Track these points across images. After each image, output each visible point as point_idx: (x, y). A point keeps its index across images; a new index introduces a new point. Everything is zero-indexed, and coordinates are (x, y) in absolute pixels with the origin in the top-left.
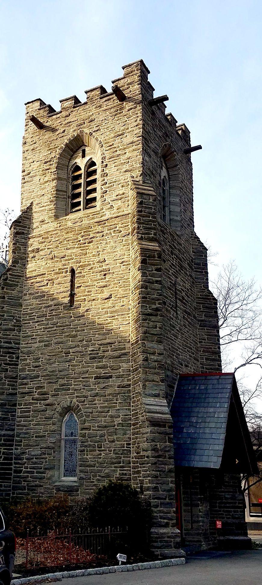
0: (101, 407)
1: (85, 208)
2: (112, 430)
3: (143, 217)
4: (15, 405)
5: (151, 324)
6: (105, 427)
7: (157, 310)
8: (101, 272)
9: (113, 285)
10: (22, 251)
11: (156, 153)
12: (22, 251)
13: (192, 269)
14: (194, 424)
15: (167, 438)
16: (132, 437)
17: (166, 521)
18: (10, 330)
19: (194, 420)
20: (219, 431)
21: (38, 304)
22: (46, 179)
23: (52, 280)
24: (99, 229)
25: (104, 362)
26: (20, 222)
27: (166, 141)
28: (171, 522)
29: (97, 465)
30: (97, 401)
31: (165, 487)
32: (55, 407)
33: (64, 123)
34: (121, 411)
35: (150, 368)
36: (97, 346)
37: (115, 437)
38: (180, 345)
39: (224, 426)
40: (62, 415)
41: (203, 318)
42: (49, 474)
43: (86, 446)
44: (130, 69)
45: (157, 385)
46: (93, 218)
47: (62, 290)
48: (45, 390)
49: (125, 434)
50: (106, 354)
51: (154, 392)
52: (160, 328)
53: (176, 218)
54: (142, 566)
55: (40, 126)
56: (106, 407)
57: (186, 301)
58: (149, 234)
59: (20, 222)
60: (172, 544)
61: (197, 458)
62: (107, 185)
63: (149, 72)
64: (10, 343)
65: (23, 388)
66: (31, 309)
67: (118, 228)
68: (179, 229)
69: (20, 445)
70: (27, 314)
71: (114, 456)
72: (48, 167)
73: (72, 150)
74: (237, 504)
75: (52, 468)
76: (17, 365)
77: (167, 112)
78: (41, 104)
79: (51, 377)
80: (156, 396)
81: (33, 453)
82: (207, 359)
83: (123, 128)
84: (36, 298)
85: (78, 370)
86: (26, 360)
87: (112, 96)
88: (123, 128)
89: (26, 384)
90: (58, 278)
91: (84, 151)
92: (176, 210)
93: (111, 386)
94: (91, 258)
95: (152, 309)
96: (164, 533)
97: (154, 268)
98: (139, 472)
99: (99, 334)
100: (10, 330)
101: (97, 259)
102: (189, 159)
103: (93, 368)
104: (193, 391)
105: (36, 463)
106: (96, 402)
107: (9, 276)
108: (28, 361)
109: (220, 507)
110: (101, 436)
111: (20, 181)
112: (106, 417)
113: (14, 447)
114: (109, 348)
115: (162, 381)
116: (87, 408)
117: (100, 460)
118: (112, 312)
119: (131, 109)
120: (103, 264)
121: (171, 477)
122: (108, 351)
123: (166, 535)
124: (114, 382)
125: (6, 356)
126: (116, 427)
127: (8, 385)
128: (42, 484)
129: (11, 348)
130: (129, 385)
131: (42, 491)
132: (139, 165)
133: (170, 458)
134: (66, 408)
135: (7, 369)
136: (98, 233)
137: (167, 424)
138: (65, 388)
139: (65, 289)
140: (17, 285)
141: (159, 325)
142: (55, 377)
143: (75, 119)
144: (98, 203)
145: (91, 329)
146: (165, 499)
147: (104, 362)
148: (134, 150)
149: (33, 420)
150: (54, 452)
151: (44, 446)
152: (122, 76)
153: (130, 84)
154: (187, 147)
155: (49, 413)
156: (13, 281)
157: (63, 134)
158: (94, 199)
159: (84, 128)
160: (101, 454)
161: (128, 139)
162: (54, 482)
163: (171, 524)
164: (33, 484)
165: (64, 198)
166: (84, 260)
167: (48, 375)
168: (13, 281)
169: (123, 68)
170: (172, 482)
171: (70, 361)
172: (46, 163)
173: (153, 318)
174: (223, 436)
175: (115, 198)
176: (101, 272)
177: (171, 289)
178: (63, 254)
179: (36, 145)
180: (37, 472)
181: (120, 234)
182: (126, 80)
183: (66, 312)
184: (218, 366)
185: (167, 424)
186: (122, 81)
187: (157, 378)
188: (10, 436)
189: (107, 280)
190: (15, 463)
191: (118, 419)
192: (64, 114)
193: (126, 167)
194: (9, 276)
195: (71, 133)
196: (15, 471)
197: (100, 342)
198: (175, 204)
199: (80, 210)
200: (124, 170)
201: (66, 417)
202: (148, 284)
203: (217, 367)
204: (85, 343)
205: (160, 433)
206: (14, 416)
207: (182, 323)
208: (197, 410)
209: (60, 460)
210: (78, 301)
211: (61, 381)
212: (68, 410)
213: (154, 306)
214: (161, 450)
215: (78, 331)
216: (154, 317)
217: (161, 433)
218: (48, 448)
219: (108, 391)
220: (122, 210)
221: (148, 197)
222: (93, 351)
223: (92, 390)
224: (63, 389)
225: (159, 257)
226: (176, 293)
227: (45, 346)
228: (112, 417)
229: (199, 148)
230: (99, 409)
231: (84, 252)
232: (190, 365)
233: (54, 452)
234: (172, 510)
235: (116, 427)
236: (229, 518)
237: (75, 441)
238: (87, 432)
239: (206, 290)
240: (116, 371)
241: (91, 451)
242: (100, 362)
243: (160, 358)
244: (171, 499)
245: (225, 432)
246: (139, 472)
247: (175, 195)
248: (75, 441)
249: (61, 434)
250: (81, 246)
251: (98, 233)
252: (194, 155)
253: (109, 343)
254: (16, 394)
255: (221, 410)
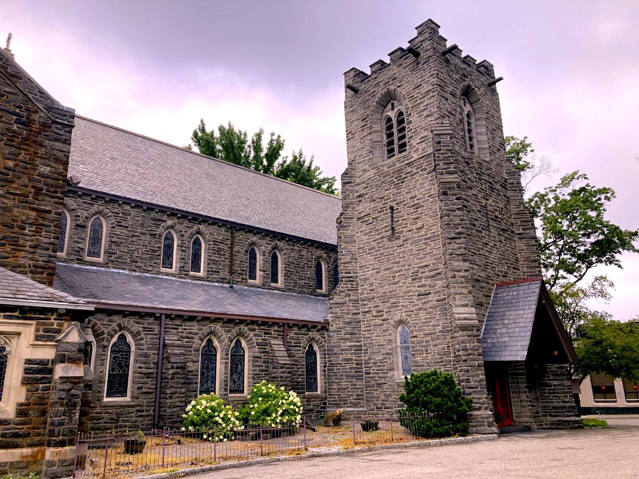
0: (424, 319)
1: (400, 152)
2: (434, 336)
3: (442, 154)
4: (360, 322)
5: (456, 246)
6: (429, 334)
7: (460, 233)
8: (414, 206)
9: (424, 216)
10: (351, 197)
11: (453, 95)
12: (351, 197)
13: (506, 189)
14: (506, 326)
15: (475, 339)
16: (450, 340)
17: (479, 405)
18: (348, 263)
19: (506, 322)
20: (526, 329)
21: (368, 239)
22: (365, 134)
23: (376, 218)
24: (409, 169)
25: (423, 282)
26: (347, 174)
27: (465, 81)
28: (484, 406)
29: (426, 365)
30: (422, 314)
31: (476, 378)
32: (390, 321)
33: (373, 84)
34: (440, 321)
35: (458, 283)
36: (416, 269)
37: (438, 342)
38: (495, 259)
39: (531, 324)
40: (396, 327)
41: (520, 232)
42: (390, 374)
43: (416, 351)
44: (421, 29)
45: (465, 297)
46: (404, 161)
47: (385, 225)
48: (380, 308)
49: (445, 339)
50: (424, 275)
51: (463, 303)
52: (464, 248)
53: (484, 146)
54: (455, 441)
55: (356, 91)
56: (428, 318)
57: (501, 219)
58: (449, 168)
59: (347, 174)
60: (486, 423)
61: (507, 353)
62: (412, 131)
63: (439, 27)
64: (350, 273)
65: (364, 308)
66: (363, 244)
67: (424, 167)
68: (488, 155)
69: (367, 353)
70: (361, 248)
71: (438, 357)
72: (365, 124)
73: (383, 106)
74: (566, 390)
75: (392, 369)
76: (358, 290)
77: (463, 55)
78: (355, 71)
79: (385, 298)
80: (465, 306)
81: (377, 359)
82: (527, 267)
83: (421, 80)
84: (366, 234)
85: (404, 289)
86: (363, 285)
87: (409, 55)
88: (421, 80)
89: (366, 305)
90: (381, 216)
91: (393, 104)
92: (483, 139)
93: (430, 301)
94: (404, 196)
95: (456, 233)
96: (478, 415)
97: (454, 197)
98: (456, 368)
99: (417, 259)
100: (348, 263)
101: (410, 195)
102: (494, 91)
103: (415, 288)
104: (507, 298)
105: (379, 366)
106: (420, 315)
107: (343, 219)
108: (366, 286)
109: (342, 375)
110: (427, 342)
111: (345, 138)
112: (429, 326)
113: (363, 355)
114: (426, 270)
115: (470, 293)
116: (414, 320)
117: (427, 361)
118: (425, 239)
119: (425, 63)
120: (415, 199)
121: (481, 370)
122: (425, 272)
123: (479, 417)
124: (433, 298)
125: (347, 284)
126: (438, 334)
127: (352, 306)
128: (386, 382)
129: (351, 277)
130: (445, 299)
131: (387, 387)
132: (436, 110)
133: (479, 355)
134: (398, 322)
135: (350, 294)
136: (408, 173)
137: (474, 329)
138: (395, 305)
139: (387, 225)
140: (350, 226)
141: (462, 246)
142: (387, 297)
143: (382, 79)
144: (408, 148)
145: (411, 255)
146: (477, 388)
147: (423, 282)
148: (431, 97)
149: (374, 333)
150: (393, 357)
151: (385, 352)
152: (416, 35)
153: (423, 41)
154: (491, 80)
155: (385, 326)
156: (347, 223)
157: (373, 94)
158: (405, 143)
159: (390, 85)
160: (428, 356)
161: (425, 88)
162: (395, 380)
163: (483, 408)
164: (380, 382)
165: (380, 147)
166: (400, 198)
167: (381, 296)
168: (347, 223)
169: (416, 29)
170: (482, 374)
171: (397, 283)
172: (363, 120)
173: (458, 241)
174: (529, 334)
175: (419, 141)
176: (414, 206)
177: (480, 212)
178: (382, 196)
179: (354, 107)
180: (382, 373)
181: (426, 172)
182: (419, 38)
183: (389, 243)
184: (539, 271)
185: (474, 329)
186: (416, 40)
187: (465, 291)
188: (359, 346)
189: (419, 212)
190: (365, 367)
191: (439, 327)
192: (373, 76)
193: (426, 113)
194: (343, 219)
195: (381, 91)
196: (366, 373)
197: (418, 266)
198: (481, 134)
199: (394, 155)
200: (425, 115)
201: (400, 329)
202: (450, 212)
203: (538, 273)
204: (406, 267)
205: (468, 336)
206: (360, 330)
207: (497, 239)
208: (509, 313)
209: (398, 363)
210: (398, 233)
211: (392, 300)
212: (401, 322)
213: (457, 231)
214: (471, 349)
215: (401, 258)
216: (459, 240)
217: (470, 336)
218: (387, 354)
219: (428, 306)
220: (426, 150)
221: (445, 136)
222: (413, 273)
223: (416, 305)
224: (394, 307)
225: (458, 188)
226: (487, 214)
227: (377, 272)
228: (433, 326)
229: (500, 79)
230: (423, 321)
231: (399, 191)
232: (509, 275)
233: (393, 357)
234: (484, 396)
235: (438, 334)
236: (559, 402)
237: (408, 348)
238: (416, 339)
239: (522, 206)
240: (433, 288)
241: (420, 354)
242: (420, 282)
243: (466, 274)
244: (482, 388)
245: (531, 330)
246: (456, 368)
247: (480, 126)
248: (408, 348)
249: (396, 343)
250: (397, 186)
251: (408, 173)
252: (498, 85)
253: (426, 266)
254: (359, 313)
255: (529, 311)
